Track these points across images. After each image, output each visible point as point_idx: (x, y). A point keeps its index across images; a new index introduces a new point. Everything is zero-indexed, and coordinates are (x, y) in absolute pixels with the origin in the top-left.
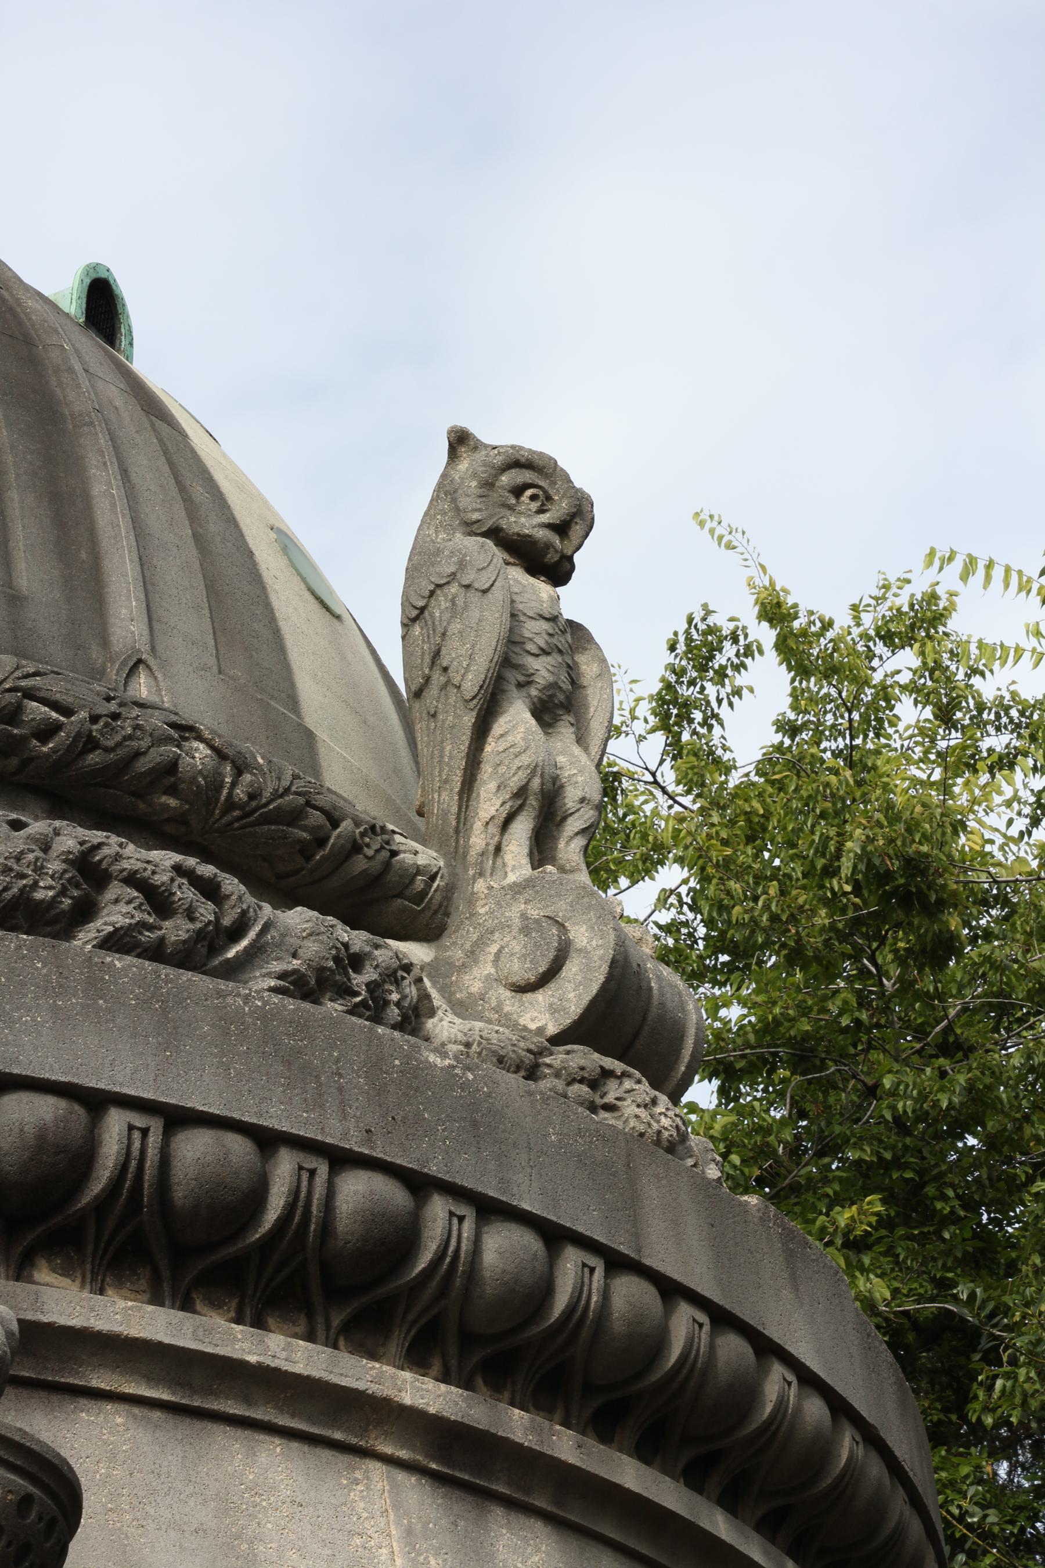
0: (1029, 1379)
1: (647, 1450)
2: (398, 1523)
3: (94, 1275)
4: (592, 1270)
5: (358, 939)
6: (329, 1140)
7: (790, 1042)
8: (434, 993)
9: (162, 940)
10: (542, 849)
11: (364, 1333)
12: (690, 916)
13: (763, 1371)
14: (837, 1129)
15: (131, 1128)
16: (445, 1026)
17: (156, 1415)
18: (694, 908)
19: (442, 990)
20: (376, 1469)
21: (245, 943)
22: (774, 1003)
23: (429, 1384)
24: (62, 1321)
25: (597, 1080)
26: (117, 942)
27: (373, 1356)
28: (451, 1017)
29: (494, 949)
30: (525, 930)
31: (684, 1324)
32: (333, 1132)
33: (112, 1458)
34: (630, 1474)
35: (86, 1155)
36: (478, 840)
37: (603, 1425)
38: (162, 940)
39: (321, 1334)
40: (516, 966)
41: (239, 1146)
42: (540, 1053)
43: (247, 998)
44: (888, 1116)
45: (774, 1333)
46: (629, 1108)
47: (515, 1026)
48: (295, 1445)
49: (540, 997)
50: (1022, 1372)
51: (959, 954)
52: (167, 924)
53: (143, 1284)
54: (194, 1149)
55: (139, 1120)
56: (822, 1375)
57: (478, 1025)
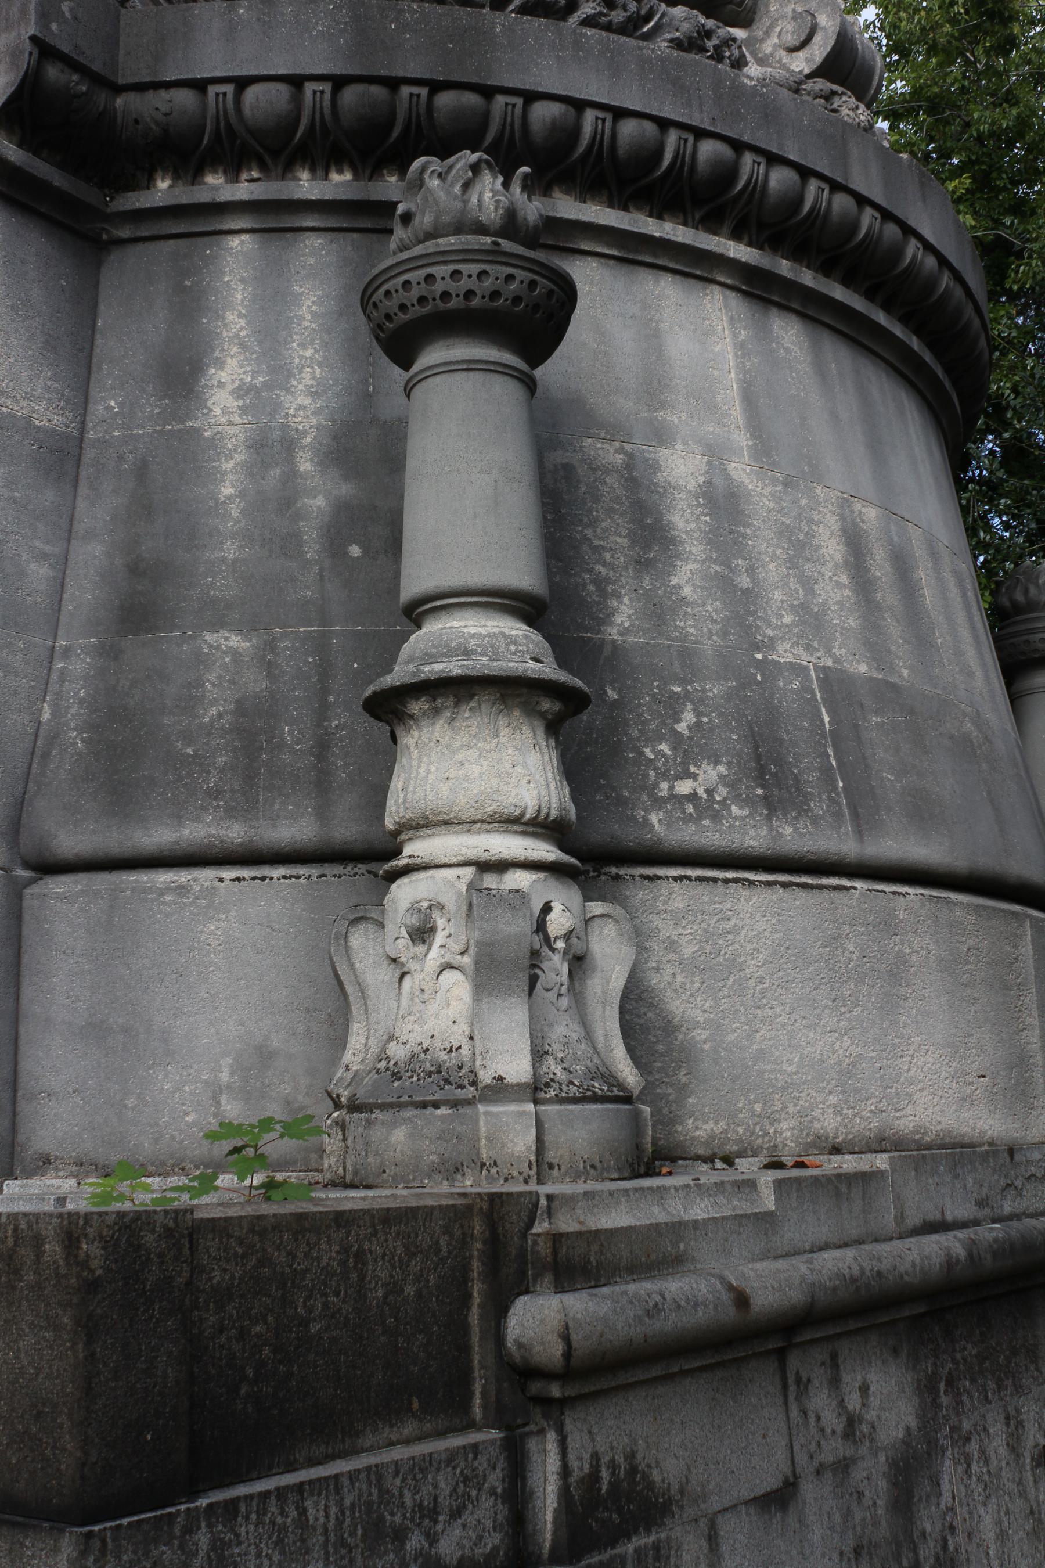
0: (1037, 265)
1: (847, 282)
2: (727, 314)
3: (581, 194)
4: (823, 190)
5: (710, 23)
6: (694, 124)
7: (928, 99)
8: (747, 55)
9: (610, 22)
11: (711, 223)
12: (879, 33)
13: (905, 242)
14: (949, 144)
15: (597, 118)
16: (753, 70)
17: (612, 262)
18: (881, 29)
19: (751, 53)
20: (717, 290)
21: (652, 23)
22: (920, 78)
23: (742, 247)
24: (566, 216)
25: (829, 96)
26: (589, 22)
27: (715, 234)
28: (755, 66)
29: (778, 29)
30: (794, 18)
31: (868, 218)
32: (698, 119)
33: (592, 283)
34: (839, 292)
35: (576, 132)
37: (826, 269)
38: (610, 22)
39: (690, 220)
40: (789, 37)
41: (650, 127)
42: (800, 83)
43: (653, 50)
44: (975, 134)
45: (912, 223)
46: (845, 111)
47: (788, 70)
48: (678, 277)
49: (801, 54)
50: (1034, 262)
51: (1018, 48)
52: (613, 13)
53: (605, 198)
54: (628, 128)
55: (601, 114)
56: (935, 245)
57: (770, 69)
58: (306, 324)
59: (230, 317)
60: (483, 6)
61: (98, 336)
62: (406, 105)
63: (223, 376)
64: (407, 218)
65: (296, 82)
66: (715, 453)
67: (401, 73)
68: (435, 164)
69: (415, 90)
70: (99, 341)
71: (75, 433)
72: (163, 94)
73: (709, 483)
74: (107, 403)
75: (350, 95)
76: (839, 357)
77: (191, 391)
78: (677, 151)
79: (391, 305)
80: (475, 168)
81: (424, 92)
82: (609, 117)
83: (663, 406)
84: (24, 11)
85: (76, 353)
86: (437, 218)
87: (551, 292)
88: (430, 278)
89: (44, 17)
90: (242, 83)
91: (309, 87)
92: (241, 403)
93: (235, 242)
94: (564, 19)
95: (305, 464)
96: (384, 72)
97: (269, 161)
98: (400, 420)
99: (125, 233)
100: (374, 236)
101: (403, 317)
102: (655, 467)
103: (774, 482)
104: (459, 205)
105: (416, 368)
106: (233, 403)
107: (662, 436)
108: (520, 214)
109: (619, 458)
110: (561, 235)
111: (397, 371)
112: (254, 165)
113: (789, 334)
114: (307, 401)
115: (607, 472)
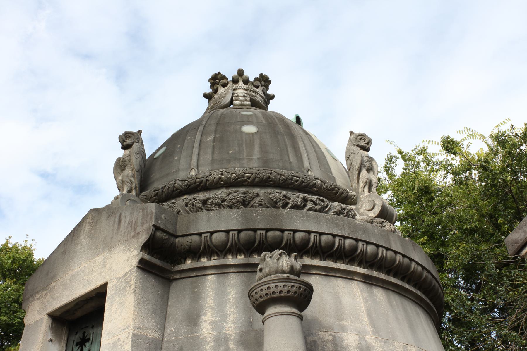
1: (395, 276)
5: (344, 206)
7: (410, 215)
10: (370, 190)
11: (351, 262)
13: (411, 263)
16: (358, 217)
17: (323, 276)
20: (355, 282)
23: (362, 269)
25: (382, 223)
26: (310, 210)
27: (353, 265)
30: (369, 202)
34: (393, 280)
35: (309, 240)
36: (360, 190)
37: (388, 273)
41: (330, 237)
45: (412, 257)
46: (387, 227)
49: (372, 211)
51: (434, 199)
54: (324, 238)
55: (316, 235)
58: (231, 301)
59: (208, 300)
60: (279, 208)
61: (168, 308)
62: (259, 236)
63: (206, 318)
64: (261, 270)
65: (227, 232)
66: (361, 334)
67: (257, 228)
68: (268, 253)
69: (261, 232)
70: (169, 309)
71: (161, 339)
72: (189, 237)
73: (360, 343)
74: (171, 328)
75: (243, 234)
76: (396, 299)
77: (196, 324)
78: (339, 243)
79: (257, 296)
80: (280, 255)
81: (264, 232)
82: (318, 235)
83: (343, 319)
84: (151, 218)
85: (161, 313)
86: (270, 269)
87: (305, 289)
88: (269, 288)
89: (157, 219)
90: (212, 233)
91: (231, 233)
92: (212, 327)
93: (210, 277)
94: (303, 209)
95: (232, 345)
96: (252, 228)
97: (220, 254)
98: (261, 329)
99: (177, 276)
100: (251, 273)
101: (261, 300)
102: (342, 340)
103: (381, 342)
104: (276, 265)
105: (266, 314)
106: (210, 327)
107: (343, 329)
108: (295, 267)
109: (331, 338)
110: (307, 270)
111: (259, 315)
112: (215, 255)
113: (379, 293)
114: (232, 325)
115: (327, 342)
